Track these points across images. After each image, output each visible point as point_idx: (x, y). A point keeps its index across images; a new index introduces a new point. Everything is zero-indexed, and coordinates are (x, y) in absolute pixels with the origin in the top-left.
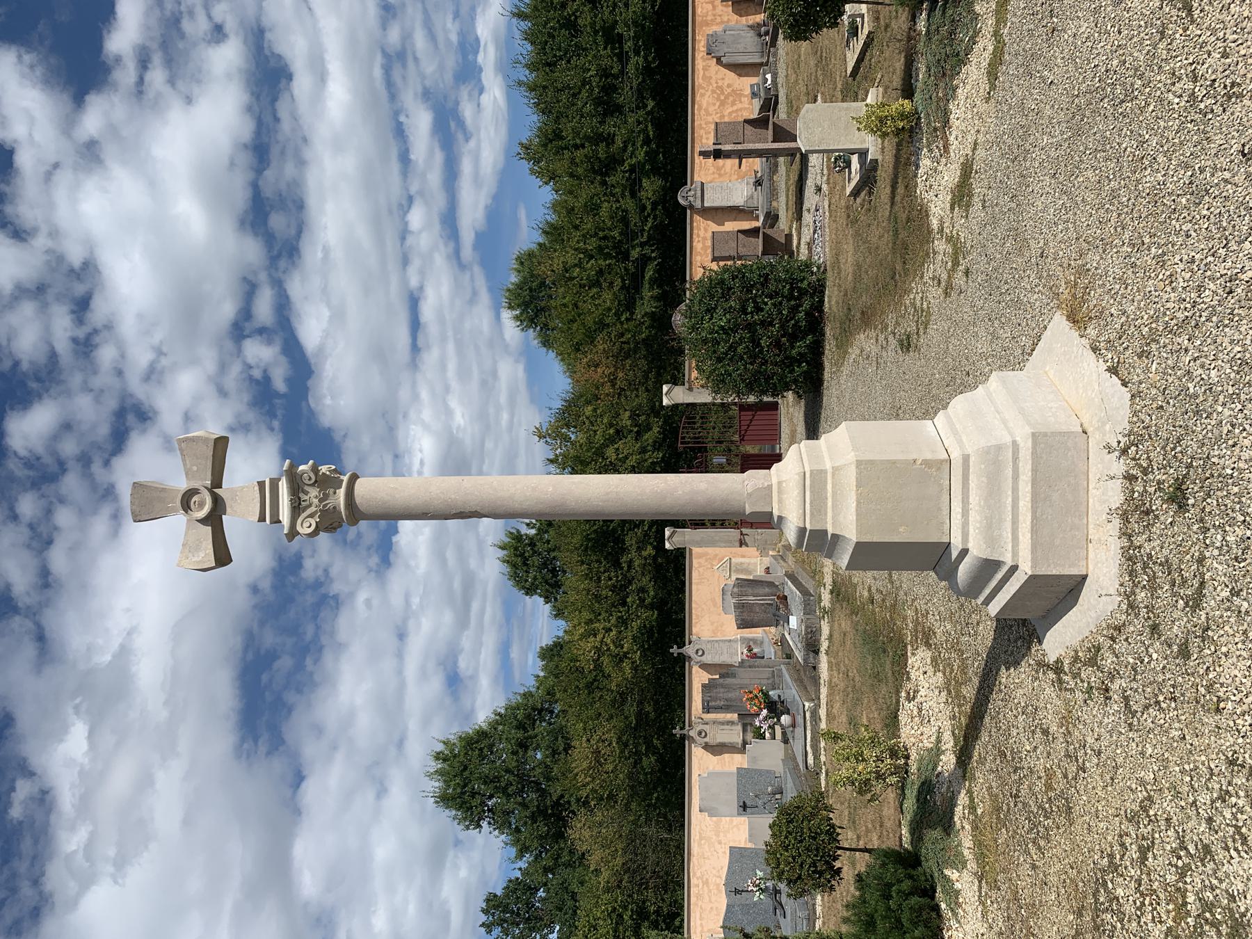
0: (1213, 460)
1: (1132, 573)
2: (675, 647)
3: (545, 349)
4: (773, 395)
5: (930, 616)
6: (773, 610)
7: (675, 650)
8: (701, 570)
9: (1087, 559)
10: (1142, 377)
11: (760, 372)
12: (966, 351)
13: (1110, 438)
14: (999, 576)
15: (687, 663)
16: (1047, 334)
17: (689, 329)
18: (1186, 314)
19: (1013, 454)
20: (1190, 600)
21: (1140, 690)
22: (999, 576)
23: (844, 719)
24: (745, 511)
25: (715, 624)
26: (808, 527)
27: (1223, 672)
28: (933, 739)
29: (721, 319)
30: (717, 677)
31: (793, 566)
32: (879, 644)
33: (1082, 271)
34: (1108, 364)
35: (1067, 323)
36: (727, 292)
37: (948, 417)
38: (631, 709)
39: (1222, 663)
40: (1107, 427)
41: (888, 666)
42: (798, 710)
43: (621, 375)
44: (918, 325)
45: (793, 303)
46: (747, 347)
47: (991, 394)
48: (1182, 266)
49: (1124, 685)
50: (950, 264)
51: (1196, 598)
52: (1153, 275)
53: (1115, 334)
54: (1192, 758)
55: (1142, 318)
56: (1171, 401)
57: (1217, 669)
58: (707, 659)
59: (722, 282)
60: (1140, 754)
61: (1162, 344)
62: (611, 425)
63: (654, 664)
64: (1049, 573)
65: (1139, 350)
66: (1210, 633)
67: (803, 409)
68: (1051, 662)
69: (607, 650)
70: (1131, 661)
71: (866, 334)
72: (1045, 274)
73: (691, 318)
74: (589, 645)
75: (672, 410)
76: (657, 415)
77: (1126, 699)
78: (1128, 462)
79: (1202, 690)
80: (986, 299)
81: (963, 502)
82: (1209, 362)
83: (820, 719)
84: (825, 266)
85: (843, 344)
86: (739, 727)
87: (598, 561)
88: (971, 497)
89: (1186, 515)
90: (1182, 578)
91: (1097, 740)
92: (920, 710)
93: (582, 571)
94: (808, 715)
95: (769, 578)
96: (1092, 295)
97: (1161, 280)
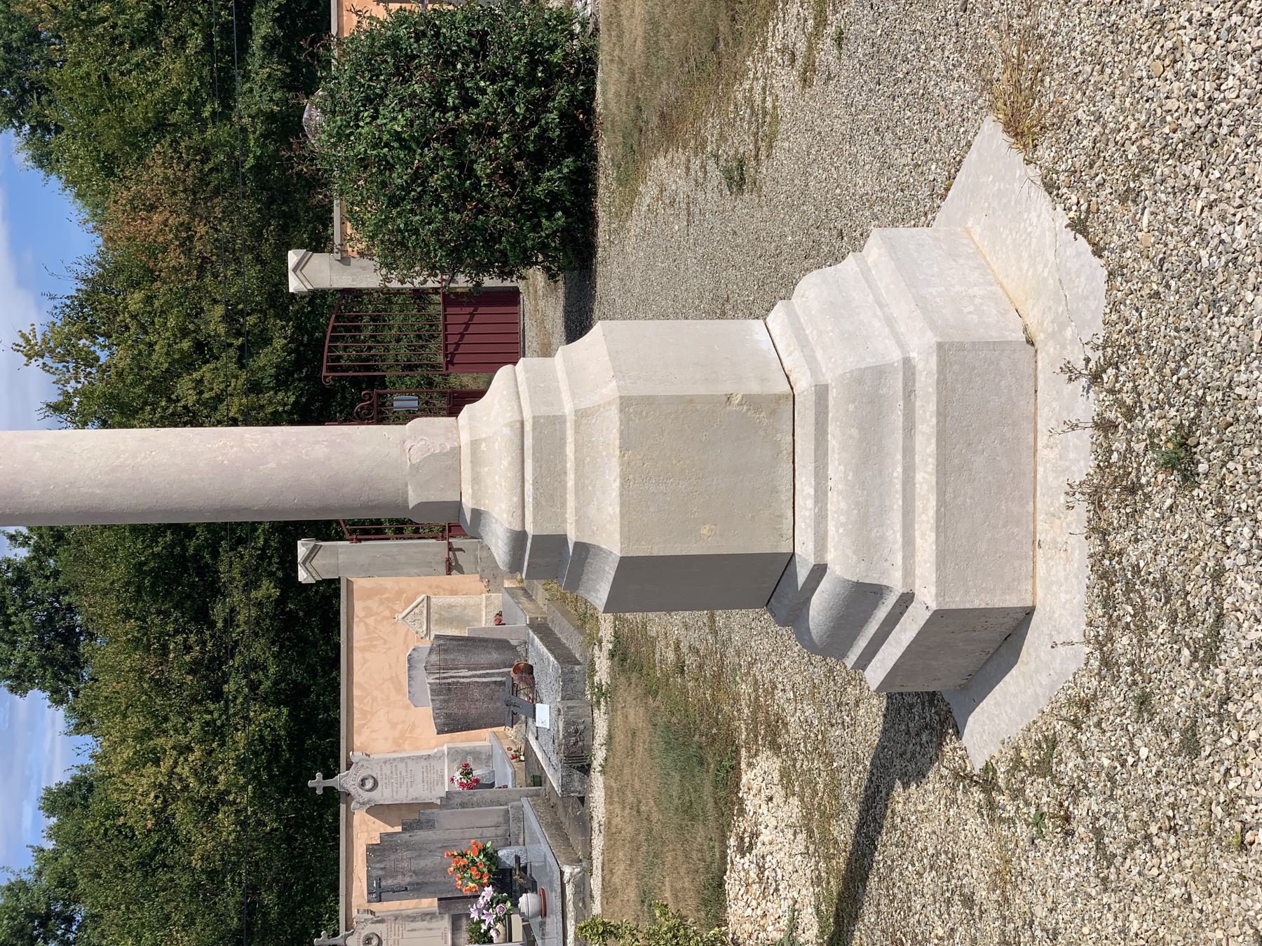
0: (1238, 390)
1: (1108, 602)
2: (319, 775)
3: (42, 173)
4: (503, 274)
5: (778, 693)
6: (505, 693)
7: (318, 783)
8: (371, 621)
9: (1034, 577)
10: (1126, 239)
11: (474, 227)
12: (838, 191)
13: (1072, 352)
14: (881, 613)
15: (343, 807)
16: (972, 156)
17: (330, 136)
18: (1197, 120)
19: (905, 385)
20: (1201, 647)
21: (1120, 816)
22: (881, 613)
23: (631, 894)
24: (406, 501)
25: (400, 727)
26: (530, 529)
27: (1250, 776)
28: (784, 923)
29: (395, 119)
30: (399, 829)
31: (545, 609)
32: (692, 751)
33: (1032, 38)
34: (1072, 214)
35: (1005, 136)
36: (404, 68)
37: (792, 315)
38: (230, 901)
39: (1249, 760)
40: (1069, 333)
41: (708, 789)
42: (551, 882)
43: (202, 230)
44: (757, 141)
45: (535, 91)
46: (448, 176)
47: (869, 270)
48: (1191, 31)
49: (1095, 808)
50: (811, 22)
51: (1208, 644)
52: (1145, 48)
53: (1083, 158)
54: (1202, 936)
55: (1128, 128)
56: (1172, 283)
57: (1242, 772)
58: (384, 795)
59: (394, 43)
60: (1120, 932)
61: (1158, 178)
62: (185, 333)
63: (278, 811)
64: (968, 606)
65: (1122, 188)
66: (1231, 707)
67: (562, 302)
68: (976, 772)
69: (182, 791)
70: (1106, 762)
71: (669, 156)
72: (969, 44)
73: (334, 113)
74: (144, 781)
75: (311, 302)
76: (282, 313)
77: (1098, 833)
78: (1101, 397)
79: (1218, 811)
80: (871, 90)
81: (816, 475)
82: (1232, 211)
83: (592, 897)
84: (596, 23)
85: (630, 177)
86: (446, 923)
87: (166, 614)
88: (830, 467)
89: (1195, 493)
90: (1188, 609)
91: (1051, 911)
92: (761, 869)
93: (126, 633)
94: (569, 890)
95: (500, 633)
96: (1047, 84)
97: (1158, 58)
